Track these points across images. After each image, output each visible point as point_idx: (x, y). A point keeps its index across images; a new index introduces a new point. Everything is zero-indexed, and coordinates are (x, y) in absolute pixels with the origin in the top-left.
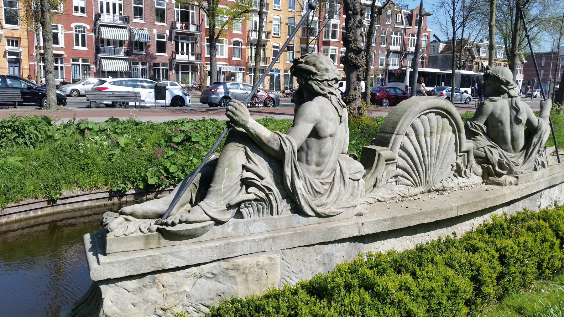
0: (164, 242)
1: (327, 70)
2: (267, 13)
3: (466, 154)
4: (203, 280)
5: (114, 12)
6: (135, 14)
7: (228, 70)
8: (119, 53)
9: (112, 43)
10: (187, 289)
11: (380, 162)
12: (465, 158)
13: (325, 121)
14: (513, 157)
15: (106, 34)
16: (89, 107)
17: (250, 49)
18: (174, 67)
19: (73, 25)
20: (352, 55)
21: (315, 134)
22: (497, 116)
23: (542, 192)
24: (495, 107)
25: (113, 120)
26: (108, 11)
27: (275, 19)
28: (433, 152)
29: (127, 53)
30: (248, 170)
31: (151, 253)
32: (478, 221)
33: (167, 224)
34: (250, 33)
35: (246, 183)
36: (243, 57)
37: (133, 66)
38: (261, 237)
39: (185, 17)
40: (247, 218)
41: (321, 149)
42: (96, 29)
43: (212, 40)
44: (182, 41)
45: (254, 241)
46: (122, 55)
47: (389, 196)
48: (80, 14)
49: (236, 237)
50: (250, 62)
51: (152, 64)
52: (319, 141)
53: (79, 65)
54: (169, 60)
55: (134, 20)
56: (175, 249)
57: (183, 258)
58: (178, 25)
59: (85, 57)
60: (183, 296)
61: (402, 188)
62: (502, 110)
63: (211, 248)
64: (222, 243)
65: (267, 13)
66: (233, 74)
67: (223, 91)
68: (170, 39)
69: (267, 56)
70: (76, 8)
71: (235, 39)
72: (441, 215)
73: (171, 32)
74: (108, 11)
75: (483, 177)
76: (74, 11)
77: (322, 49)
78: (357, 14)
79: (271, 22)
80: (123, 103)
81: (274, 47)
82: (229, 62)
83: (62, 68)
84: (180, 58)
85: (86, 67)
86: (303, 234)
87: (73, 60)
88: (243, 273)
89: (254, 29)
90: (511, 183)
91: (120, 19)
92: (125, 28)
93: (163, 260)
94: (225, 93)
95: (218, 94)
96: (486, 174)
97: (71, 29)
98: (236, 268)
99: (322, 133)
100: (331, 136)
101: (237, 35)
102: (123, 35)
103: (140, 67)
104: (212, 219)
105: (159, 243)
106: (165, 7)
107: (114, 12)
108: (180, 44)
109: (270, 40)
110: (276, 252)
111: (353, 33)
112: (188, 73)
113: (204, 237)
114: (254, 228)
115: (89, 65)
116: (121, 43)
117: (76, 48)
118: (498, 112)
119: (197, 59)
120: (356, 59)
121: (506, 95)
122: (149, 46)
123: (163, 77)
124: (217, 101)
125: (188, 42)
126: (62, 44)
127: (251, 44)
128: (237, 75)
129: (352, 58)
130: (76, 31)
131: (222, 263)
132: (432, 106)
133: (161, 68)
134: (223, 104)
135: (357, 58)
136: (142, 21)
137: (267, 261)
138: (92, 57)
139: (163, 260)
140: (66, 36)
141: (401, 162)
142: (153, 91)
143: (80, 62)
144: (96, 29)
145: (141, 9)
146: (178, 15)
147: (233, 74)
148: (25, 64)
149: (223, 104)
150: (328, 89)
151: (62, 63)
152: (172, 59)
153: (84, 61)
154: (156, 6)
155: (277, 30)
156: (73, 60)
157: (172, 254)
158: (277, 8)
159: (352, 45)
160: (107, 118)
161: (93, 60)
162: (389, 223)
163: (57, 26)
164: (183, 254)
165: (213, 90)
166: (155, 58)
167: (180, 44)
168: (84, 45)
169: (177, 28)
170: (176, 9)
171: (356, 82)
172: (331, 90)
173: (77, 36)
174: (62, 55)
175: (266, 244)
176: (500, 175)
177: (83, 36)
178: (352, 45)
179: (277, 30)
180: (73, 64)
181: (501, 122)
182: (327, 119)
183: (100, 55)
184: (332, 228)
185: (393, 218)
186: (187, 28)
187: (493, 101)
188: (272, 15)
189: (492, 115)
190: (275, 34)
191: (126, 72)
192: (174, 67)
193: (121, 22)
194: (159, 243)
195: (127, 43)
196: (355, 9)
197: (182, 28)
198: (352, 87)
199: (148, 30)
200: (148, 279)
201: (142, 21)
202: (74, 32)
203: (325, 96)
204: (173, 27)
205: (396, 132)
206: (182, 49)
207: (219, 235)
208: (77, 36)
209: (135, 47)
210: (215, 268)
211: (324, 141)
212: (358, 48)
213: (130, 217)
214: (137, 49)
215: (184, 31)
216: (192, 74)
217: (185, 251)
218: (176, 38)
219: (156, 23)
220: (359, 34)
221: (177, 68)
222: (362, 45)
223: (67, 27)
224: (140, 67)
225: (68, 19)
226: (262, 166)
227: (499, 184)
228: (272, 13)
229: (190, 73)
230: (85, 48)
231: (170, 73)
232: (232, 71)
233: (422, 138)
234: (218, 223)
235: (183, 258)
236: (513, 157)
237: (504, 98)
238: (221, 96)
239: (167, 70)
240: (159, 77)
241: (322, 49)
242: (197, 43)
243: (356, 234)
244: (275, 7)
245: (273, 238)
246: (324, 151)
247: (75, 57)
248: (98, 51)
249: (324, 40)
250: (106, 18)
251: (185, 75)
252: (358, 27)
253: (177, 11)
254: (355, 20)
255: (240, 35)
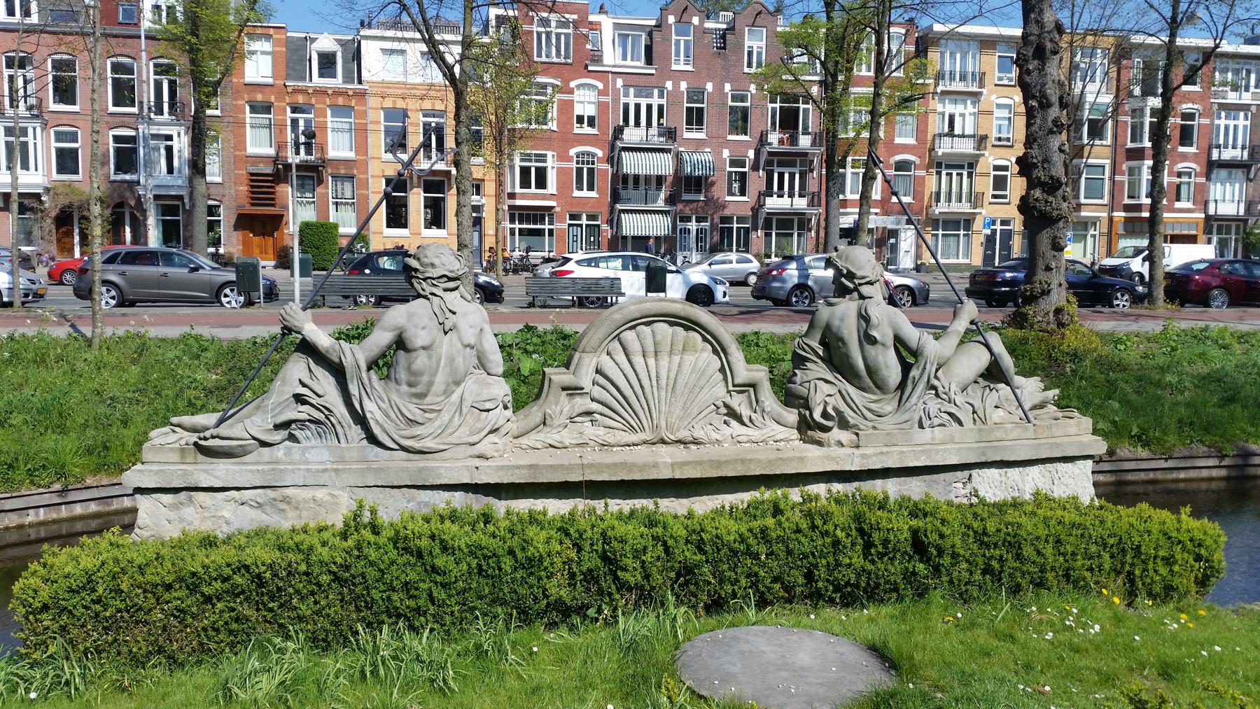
0: (201, 457)
1: (433, 265)
2: (981, 93)
3: (751, 390)
4: (245, 507)
5: (649, 124)
6: (689, 122)
7: (881, 225)
8: (655, 201)
9: (642, 181)
10: (226, 514)
11: (552, 390)
12: (749, 396)
13: (414, 330)
14: (875, 401)
15: (633, 164)
16: (532, 305)
17: (935, 177)
18: (761, 222)
19: (572, 152)
20: (1037, 193)
21: (400, 344)
22: (835, 330)
23: (975, 472)
24: (832, 314)
25: (529, 328)
26: (637, 124)
27: (999, 106)
28: (663, 382)
29: (671, 200)
30: (304, 385)
31: (183, 467)
32: (743, 498)
33: (205, 439)
34: (937, 141)
35: (299, 399)
36: (918, 195)
37: (680, 225)
38: (321, 467)
39: (789, 121)
40: (305, 443)
41: (410, 364)
42: (613, 159)
43: (833, 163)
44: (781, 170)
45: (308, 470)
46: (660, 204)
47: (574, 442)
48: (587, 130)
49: (289, 464)
50: (934, 204)
51: (717, 220)
52: (407, 355)
53: (581, 226)
54: (752, 209)
55: (687, 135)
56: (212, 467)
57: (217, 478)
58: (774, 138)
59: (593, 211)
60: (221, 521)
61: (601, 431)
62: (842, 320)
63: (252, 471)
64: (266, 467)
65: (981, 93)
66: (894, 233)
67: (796, 273)
68: (755, 167)
69: (978, 188)
70: (580, 119)
71: (898, 158)
72: (630, 471)
73: (758, 154)
74: (637, 124)
75: (799, 429)
76: (576, 125)
77: (1124, 167)
78: (1049, 105)
79: (991, 113)
80: (598, 299)
81: (996, 168)
82: (883, 208)
83: (551, 232)
84: (773, 203)
85: (593, 230)
86: (380, 470)
87: (573, 217)
88: (297, 508)
89: (946, 130)
90: (841, 444)
91: (660, 135)
92: (668, 151)
93: (195, 477)
94: (800, 277)
95: (783, 281)
96: (804, 426)
97: (570, 159)
98: (286, 500)
99: (409, 346)
100: (424, 348)
101: (905, 148)
102: (662, 165)
103: (693, 226)
104: (254, 438)
105: (195, 458)
106: (748, 104)
107: (649, 124)
108: (776, 176)
109: (987, 153)
110: (343, 489)
111: (1040, 147)
112: (791, 235)
113: (247, 458)
114: (312, 456)
115: (598, 226)
116: (660, 180)
117: (577, 193)
118: (836, 323)
119: (811, 204)
120: (1047, 202)
121: (856, 294)
122: (713, 184)
123: (738, 245)
124: (782, 295)
125: (792, 170)
126: (552, 187)
127: (939, 165)
128: (902, 235)
129: (1036, 200)
130: (578, 163)
131: (269, 491)
132: (660, 312)
133: (735, 226)
134: (794, 299)
135: (1051, 199)
136: (701, 136)
137: (327, 498)
138: (605, 209)
139: (195, 477)
140: (561, 172)
141: (597, 392)
142: (641, 275)
143: (584, 221)
144: (613, 159)
145: (700, 110)
146: (773, 116)
147: (894, 233)
148: (489, 227)
149: (794, 299)
150: (429, 289)
151: (551, 223)
152: (759, 205)
153: (590, 217)
154: (730, 103)
155: (1004, 129)
156: (573, 217)
157: (204, 471)
158: (1006, 82)
159: (1039, 173)
160: (521, 326)
161: (606, 216)
162: (525, 472)
163: (545, 155)
164: (218, 473)
165: (775, 273)
166: (724, 206)
167: (776, 176)
168: (591, 188)
169: (770, 144)
170: (770, 106)
171: (1050, 253)
172: (435, 290)
173: (580, 171)
174: (553, 207)
175: (326, 476)
176: (827, 429)
177: (591, 171)
178: (1039, 173)
179: (1004, 129)
180: (570, 225)
181: (842, 340)
182: (416, 326)
183: (619, 207)
184: (424, 468)
185: (532, 467)
186: (794, 140)
187: (831, 305)
188: (993, 97)
189: (828, 328)
190: (1000, 139)
191: (665, 237)
192: (761, 222)
193: (662, 139)
194: (195, 458)
195: (670, 179)
196: (1044, 96)
197: (781, 142)
198: (1041, 265)
199: (708, 151)
200: (183, 495)
201: (701, 136)
202: (575, 165)
203: (425, 297)
204: (762, 141)
205: (580, 349)
206: (781, 186)
207: (266, 459)
208: (580, 171)
209: (687, 186)
210: (259, 495)
211: (414, 354)
212: (1052, 178)
213: (177, 429)
214: (688, 191)
215: (786, 148)
216: (799, 235)
217: (221, 472)
218: (769, 163)
219: (730, 137)
220: (1056, 148)
221: (767, 225)
222: (1058, 171)
223: (563, 157)
224: (693, 226)
225: (564, 140)
226: (325, 383)
227: (819, 443)
228: (991, 93)
229: (796, 235)
230: (593, 194)
231: (753, 235)
232: (890, 227)
233: (638, 360)
234: (264, 444)
235: (217, 478)
236: (875, 401)
237: (850, 299)
238: (790, 285)
239: (747, 231)
240: (730, 245)
241: (1124, 167)
242: (812, 171)
243: (465, 481)
244: (1000, 79)
245: (336, 471)
246: (414, 367)
247: (575, 210)
248: (616, 198)
249: (1130, 145)
250: (632, 135)
251: (783, 240)
252: (1051, 132)
253: (774, 110)
254: (1044, 119)
255: (914, 146)
